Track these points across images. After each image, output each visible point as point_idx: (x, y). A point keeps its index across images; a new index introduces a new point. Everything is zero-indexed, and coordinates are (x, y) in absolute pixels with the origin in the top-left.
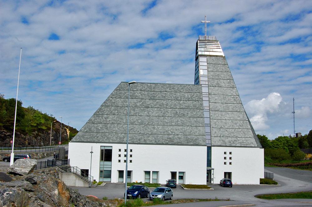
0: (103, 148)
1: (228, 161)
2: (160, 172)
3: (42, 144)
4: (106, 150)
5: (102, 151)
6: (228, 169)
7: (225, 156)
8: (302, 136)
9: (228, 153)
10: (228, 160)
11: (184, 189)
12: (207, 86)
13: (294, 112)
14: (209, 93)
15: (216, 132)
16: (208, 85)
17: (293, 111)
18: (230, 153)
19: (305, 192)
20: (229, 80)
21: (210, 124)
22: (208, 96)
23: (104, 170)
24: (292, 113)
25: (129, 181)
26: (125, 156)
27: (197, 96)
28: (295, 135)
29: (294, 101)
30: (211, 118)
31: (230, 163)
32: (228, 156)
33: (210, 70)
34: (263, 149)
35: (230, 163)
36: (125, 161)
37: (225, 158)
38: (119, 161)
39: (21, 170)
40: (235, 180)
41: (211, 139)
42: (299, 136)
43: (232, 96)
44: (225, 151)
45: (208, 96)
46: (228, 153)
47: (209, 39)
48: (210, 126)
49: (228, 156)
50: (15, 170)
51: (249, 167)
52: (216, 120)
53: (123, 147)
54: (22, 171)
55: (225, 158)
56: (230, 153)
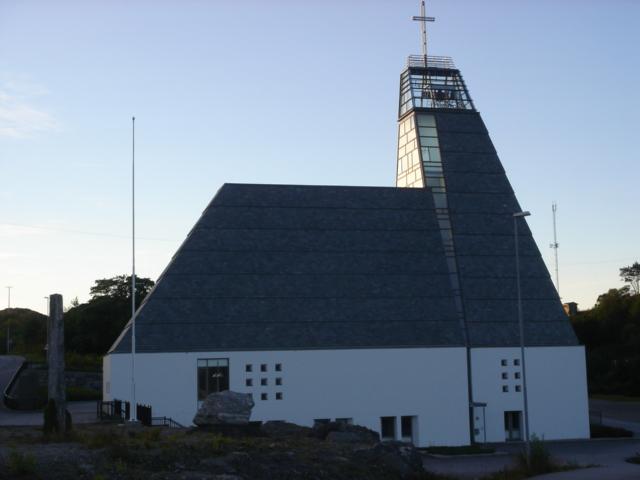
0: (203, 364)
2: (420, 420)
6: (514, 403)
7: (504, 369)
8: (581, 308)
13: (556, 246)
18: (278, 368)
24: (551, 246)
25: (407, 440)
26: (264, 382)
29: (554, 215)
31: (279, 396)
35: (279, 396)
36: (517, 389)
37: (504, 376)
39: (234, 418)
42: (67, 305)
44: (249, 363)
46: (271, 368)
47: (432, 52)
49: (511, 369)
51: (556, 393)
54: (238, 419)
55: (278, 382)
56: (278, 368)
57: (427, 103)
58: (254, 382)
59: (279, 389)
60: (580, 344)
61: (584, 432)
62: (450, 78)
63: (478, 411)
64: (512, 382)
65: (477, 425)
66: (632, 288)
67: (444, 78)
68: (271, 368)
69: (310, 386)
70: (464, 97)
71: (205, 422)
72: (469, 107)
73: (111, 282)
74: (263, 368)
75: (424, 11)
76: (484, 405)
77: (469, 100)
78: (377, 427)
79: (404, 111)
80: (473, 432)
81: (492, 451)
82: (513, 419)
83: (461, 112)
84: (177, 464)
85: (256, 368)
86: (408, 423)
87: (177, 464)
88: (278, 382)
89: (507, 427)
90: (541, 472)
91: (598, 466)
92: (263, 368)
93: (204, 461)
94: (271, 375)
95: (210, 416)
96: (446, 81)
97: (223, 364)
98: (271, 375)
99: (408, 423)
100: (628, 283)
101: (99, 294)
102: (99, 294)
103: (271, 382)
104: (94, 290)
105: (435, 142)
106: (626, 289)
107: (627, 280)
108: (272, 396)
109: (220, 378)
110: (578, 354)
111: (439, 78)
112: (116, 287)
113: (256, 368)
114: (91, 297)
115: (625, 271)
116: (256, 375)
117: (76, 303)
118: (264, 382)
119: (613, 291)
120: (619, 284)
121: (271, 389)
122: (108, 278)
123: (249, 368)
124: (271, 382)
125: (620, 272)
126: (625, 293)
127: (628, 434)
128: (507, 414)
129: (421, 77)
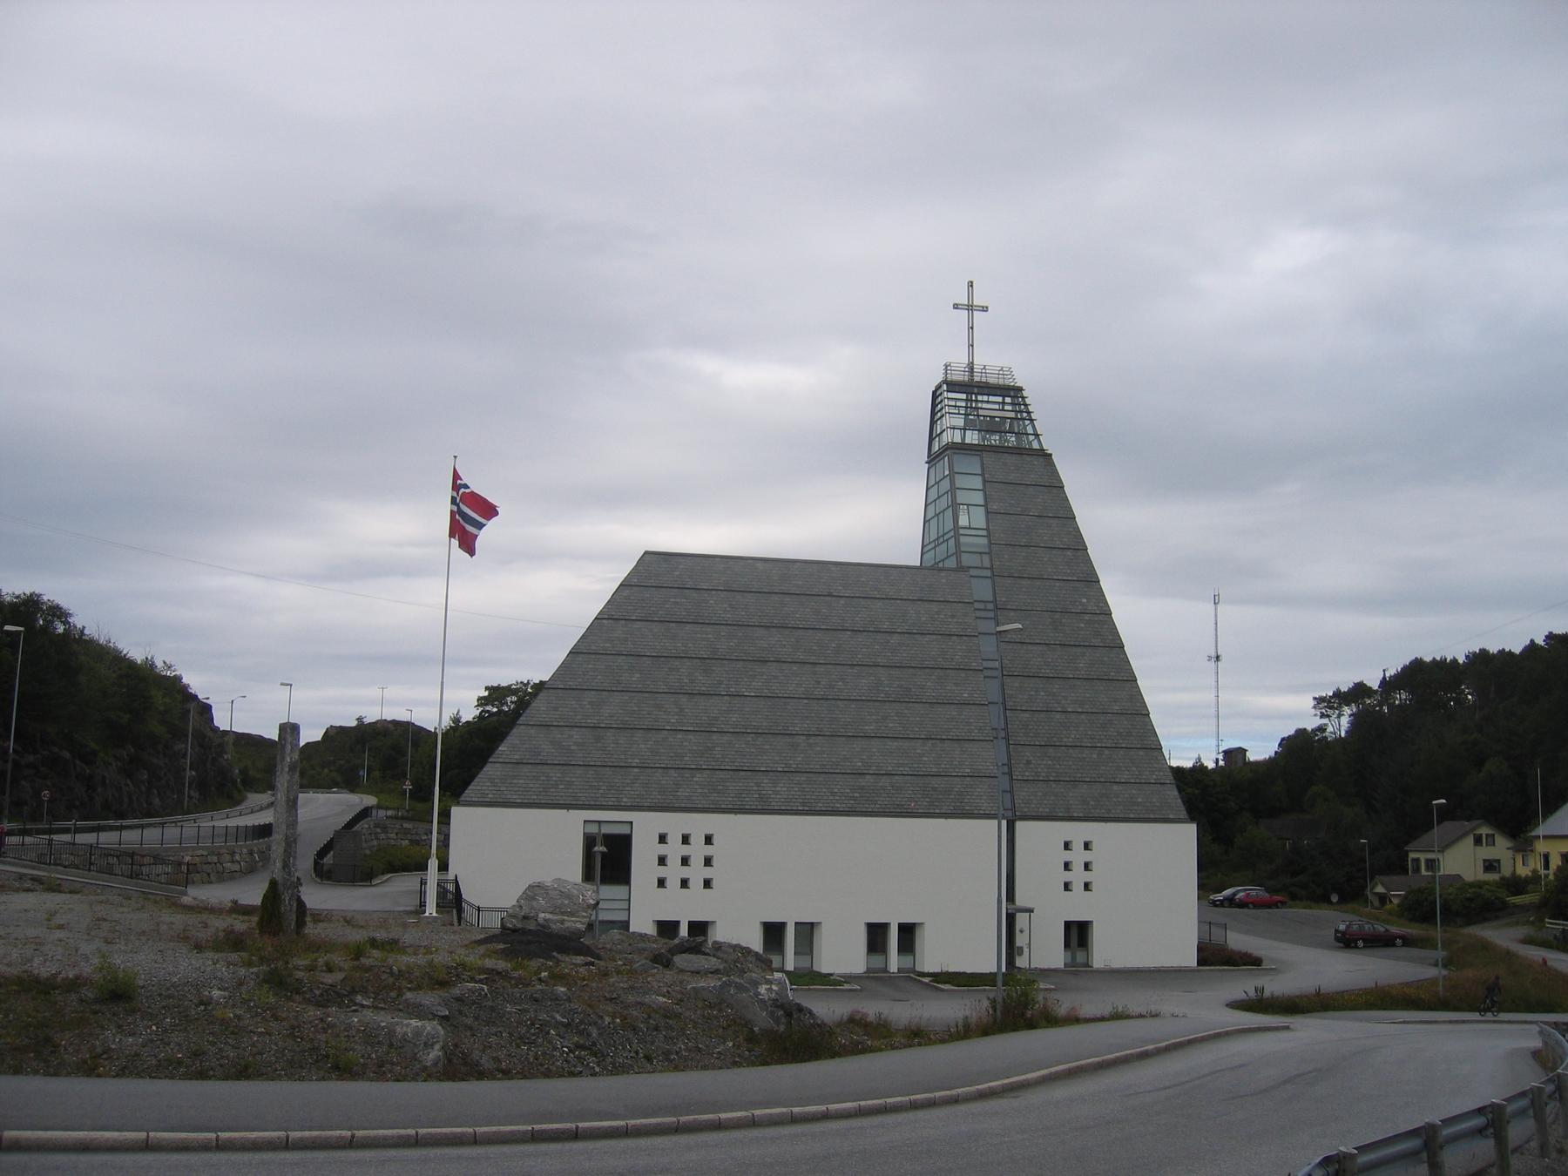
0: (593, 829)
1: (1078, 876)
2: (926, 926)
3: (157, 801)
4: (609, 839)
5: (589, 841)
8: (1252, 756)
9: (1078, 846)
10: (1078, 874)
11: (764, 1016)
12: (988, 573)
14: (995, 601)
15: (1029, 762)
16: (991, 568)
17: (1213, 654)
19: (1300, 997)
20: (1069, 553)
21: (1006, 729)
22: (991, 615)
23: (602, 922)
24: (1210, 658)
25: (804, 963)
26: (685, 861)
27: (953, 617)
28: (1221, 757)
30: (1010, 704)
31: (707, 884)
32: (1078, 856)
33: (994, 506)
34: (1192, 829)
35: (707, 884)
38: (661, 883)
39: (562, 922)
40: (1105, 952)
41: (1011, 791)
43: (1087, 617)
45: (991, 615)
46: (1078, 846)
48: (1007, 738)
49: (1078, 856)
50: (540, 921)
51: (1143, 889)
52: (1027, 715)
53: (676, 824)
54: (567, 924)
55: (708, 862)
57: (972, 437)
58: (692, 861)
59: (1088, 877)
60: (1192, 819)
61: (1192, 961)
62: (1008, 400)
63: (1021, 920)
64: (1078, 876)
65: (1020, 940)
66: (1330, 729)
67: (1000, 399)
68: (697, 840)
69: (759, 875)
70: (1030, 430)
71: (519, 926)
72: (1035, 445)
73: (508, 690)
74: (686, 840)
75: (970, 295)
76: (1031, 911)
77: (1037, 435)
78: (756, 942)
79: (936, 448)
80: (1012, 950)
81: (840, 983)
82: (1078, 934)
83: (1019, 451)
84: (359, 998)
85: (675, 839)
86: (807, 931)
87: (359, 998)
88: (708, 862)
89: (1067, 945)
90: (1015, 1028)
91: (1156, 1015)
92: (686, 840)
93: (409, 995)
94: (697, 850)
95: (525, 918)
96: (1004, 403)
97: (624, 830)
98: (697, 850)
99: (807, 931)
100: (1325, 721)
101: (489, 708)
102: (489, 708)
103: (1078, 867)
104: (482, 701)
105: (978, 498)
106: (1322, 729)
107: (1323, 716)
108: (1078, 887)
109: (603, 853)
110: (1187, 834)
111: (992, 399)
112: (515, 699)
113: (675, 839)
114: (477, 712)
115: (1320, 700)
116: (674, 850)
117: (456, 720)
118: (685, 861)
119: (1301, 733)
120: (1311, 723)
121: (696, 873)
122: (504, 684)
123: (663, 839)
124: (1078, 867)
125: (1312, 703)
126: (1320, 735)
127: (1256, 962)
128: (1068, 925)
129: (964, 396)
